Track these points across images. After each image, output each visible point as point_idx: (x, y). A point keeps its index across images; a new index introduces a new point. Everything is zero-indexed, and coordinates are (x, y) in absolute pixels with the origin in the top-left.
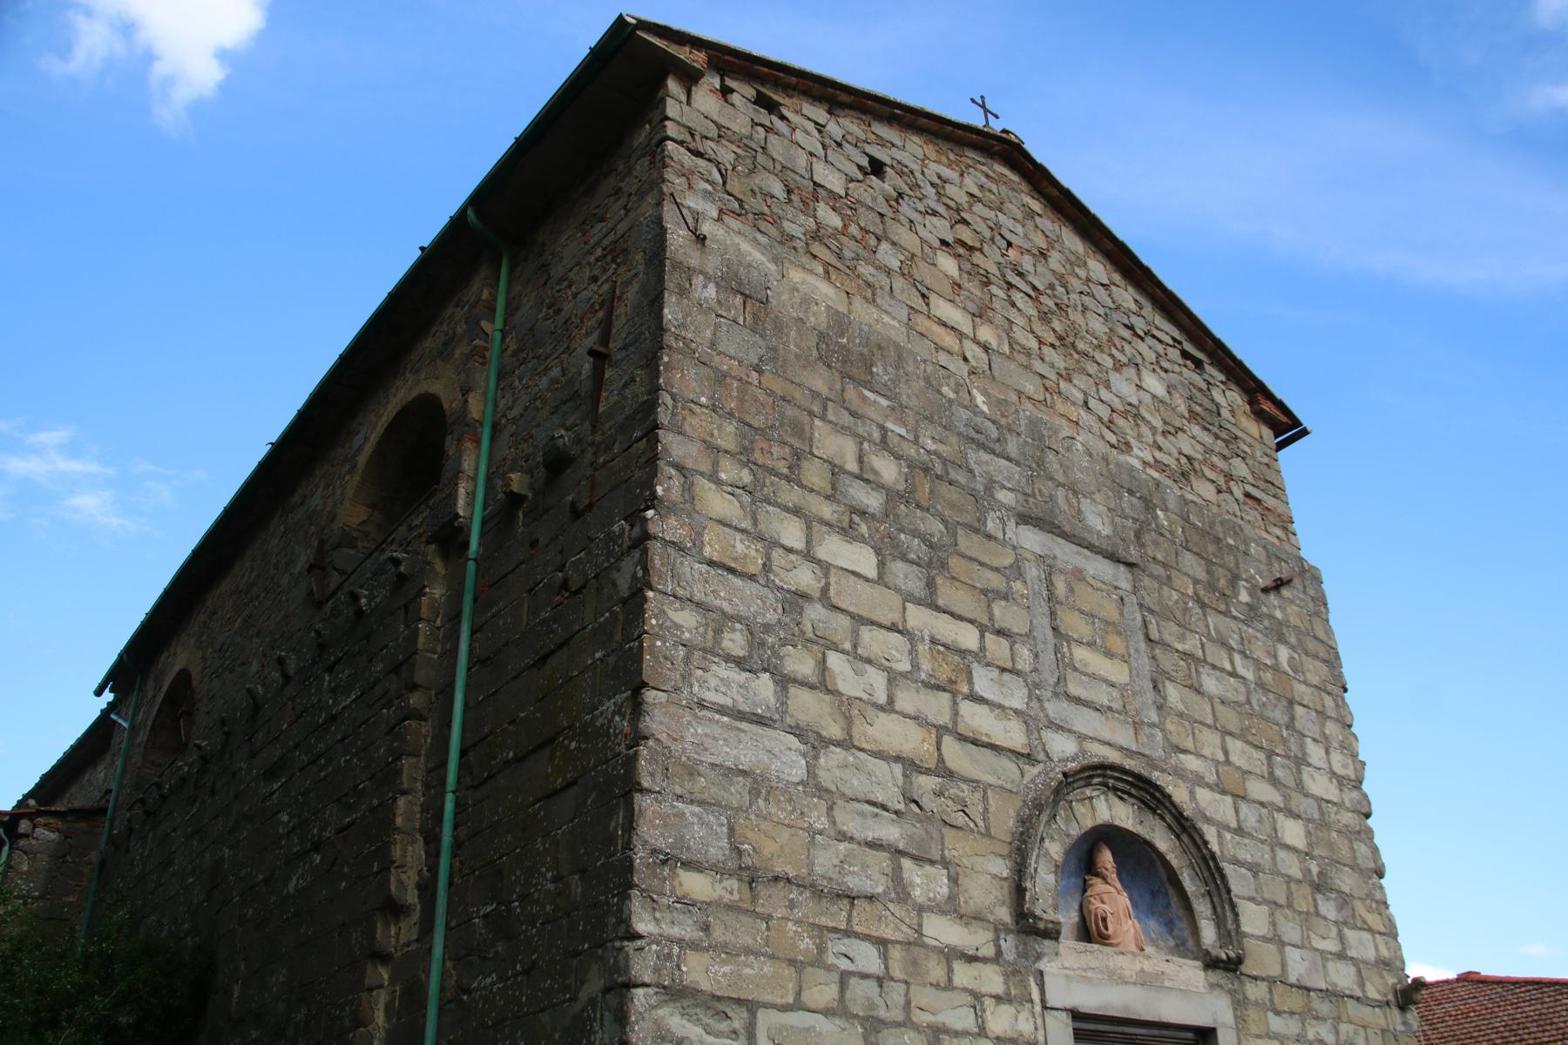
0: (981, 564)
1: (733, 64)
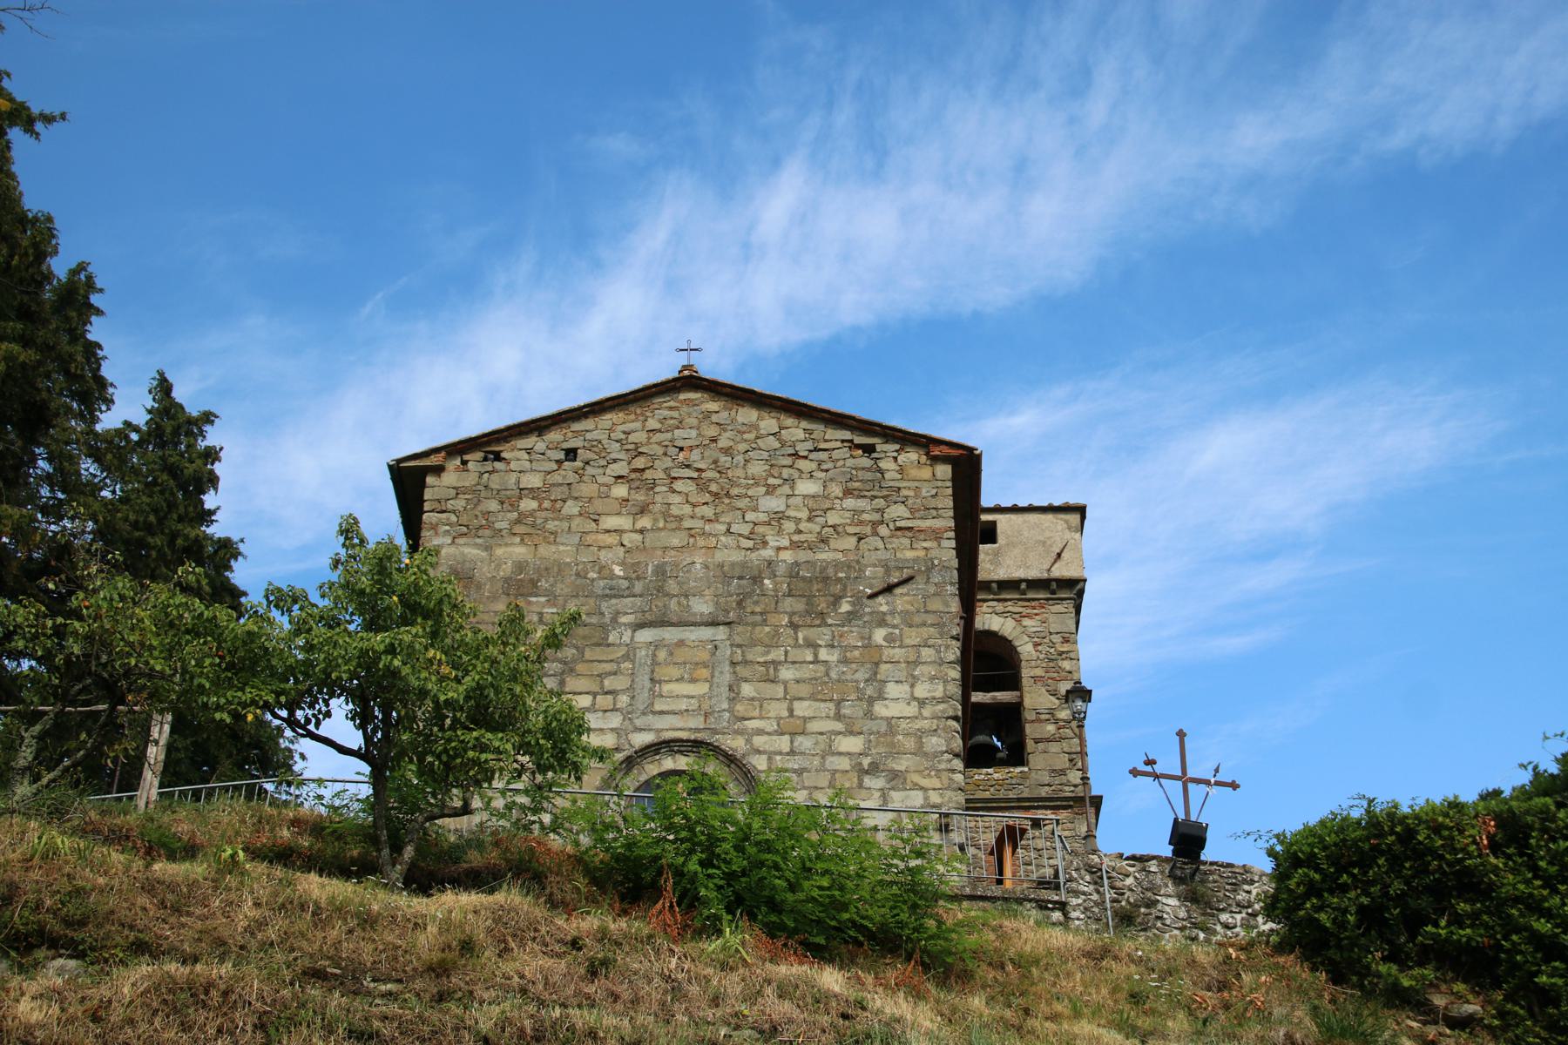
1: (459, 449)
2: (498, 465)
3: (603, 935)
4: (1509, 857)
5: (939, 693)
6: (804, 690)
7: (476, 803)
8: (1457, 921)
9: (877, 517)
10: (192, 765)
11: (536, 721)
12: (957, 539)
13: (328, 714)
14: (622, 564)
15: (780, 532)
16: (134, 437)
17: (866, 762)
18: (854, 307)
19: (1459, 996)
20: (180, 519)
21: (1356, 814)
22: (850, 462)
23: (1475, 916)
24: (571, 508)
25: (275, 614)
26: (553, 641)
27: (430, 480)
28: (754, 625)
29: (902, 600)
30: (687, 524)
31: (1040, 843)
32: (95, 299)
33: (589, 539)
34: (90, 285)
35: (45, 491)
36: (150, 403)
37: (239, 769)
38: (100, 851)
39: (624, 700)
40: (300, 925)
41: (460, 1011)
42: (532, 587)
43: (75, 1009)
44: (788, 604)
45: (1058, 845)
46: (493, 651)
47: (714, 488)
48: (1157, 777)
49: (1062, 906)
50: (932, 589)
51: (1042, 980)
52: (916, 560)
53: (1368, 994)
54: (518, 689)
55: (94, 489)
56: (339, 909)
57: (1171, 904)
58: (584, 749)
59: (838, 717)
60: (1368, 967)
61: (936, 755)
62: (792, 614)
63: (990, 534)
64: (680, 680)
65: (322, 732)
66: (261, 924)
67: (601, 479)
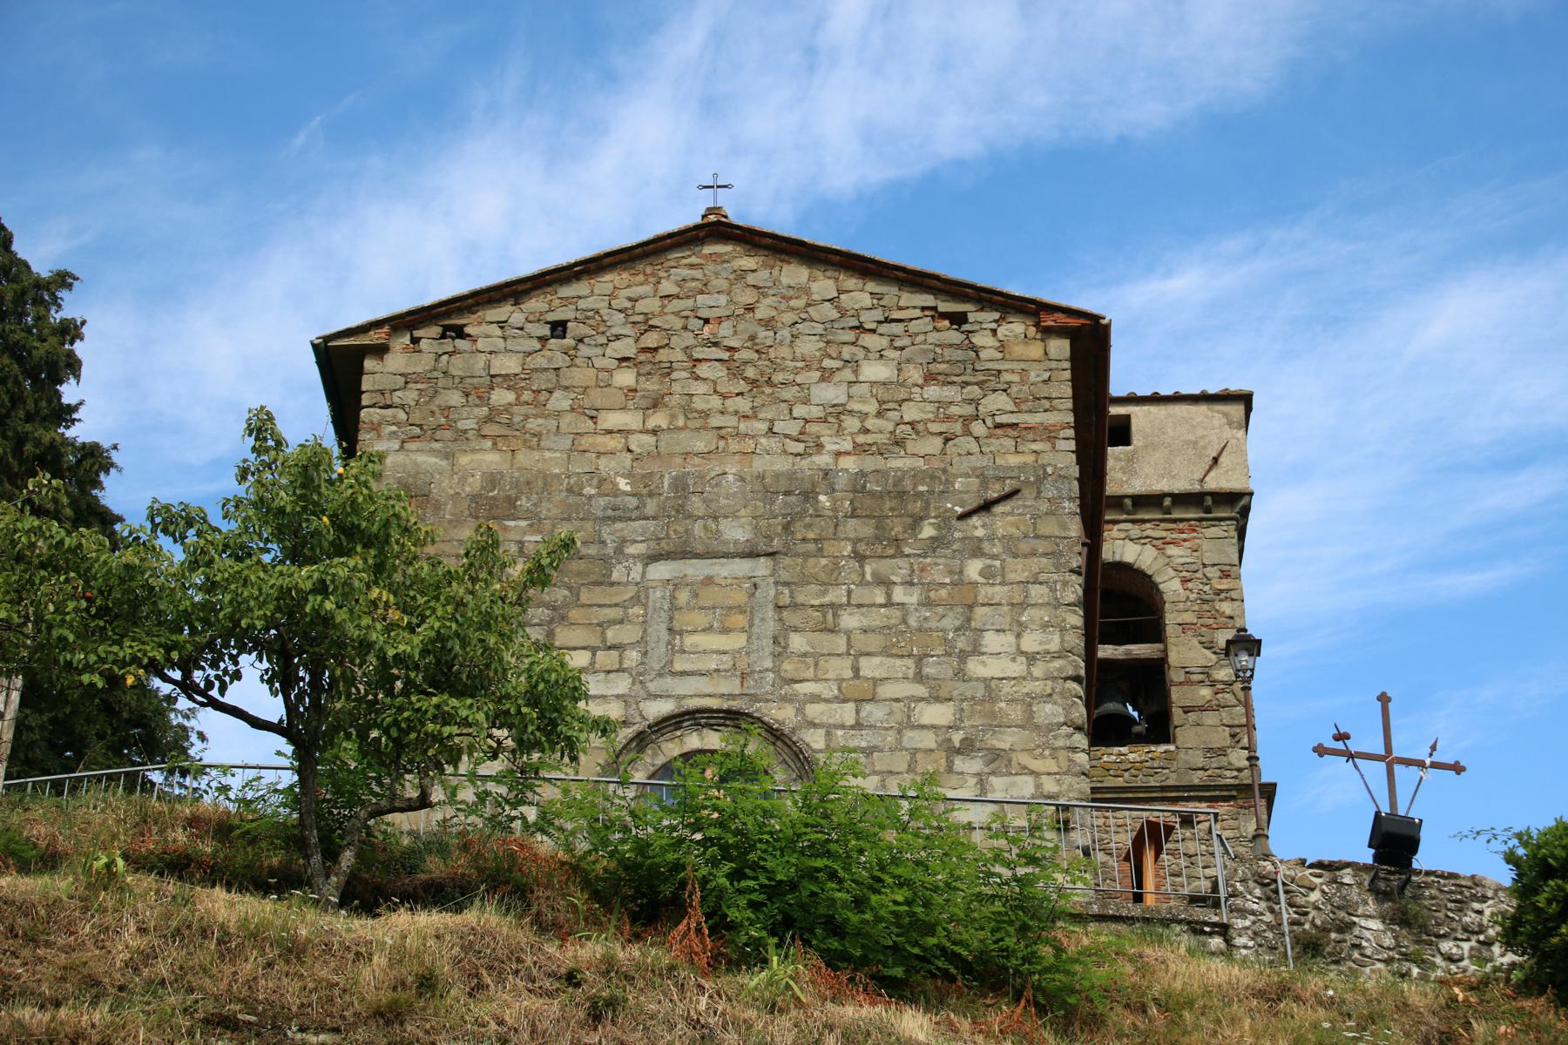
0: (600, 606)
1: (409, 322)
2: (461, 344)
3: (608, 967)
5: (1054, 646)
6: (874, 642)
7: (437, 794)
9: (969, 410)
12: (1078, 438)
13: (237, 676)
14: (629, 475)
17: (957, 738)
18: (955, 133)
20: (29, 418)
22: (933, 337)
24: (560, 401)
25: (164, 542)
26: (538, 576)
27: (369, 364)
28: (806, 556)
29: (1004, 520)
30: (715, 421)
31: (1192, 847)
33: (585, 442)
37: (116, 752)
39: (633, 656)
40: (201, 957)
42: (509, 507)
44: (852, 527)
45: (1218, 849)
46: (458, 590)
47: (750, 372)
49: (1223, 930)
51: (1197, 1027)
52: (1022, 467)
54: (492, 640)
57: (1372, 927)
58: (582, 720)
59: (919, 678)
61: (1052, 727)
62: (856, 541)
63: (1121, 433)
64: (708, 629)
65: (230, 698)
66: (148, 956)
67: (599, 362)
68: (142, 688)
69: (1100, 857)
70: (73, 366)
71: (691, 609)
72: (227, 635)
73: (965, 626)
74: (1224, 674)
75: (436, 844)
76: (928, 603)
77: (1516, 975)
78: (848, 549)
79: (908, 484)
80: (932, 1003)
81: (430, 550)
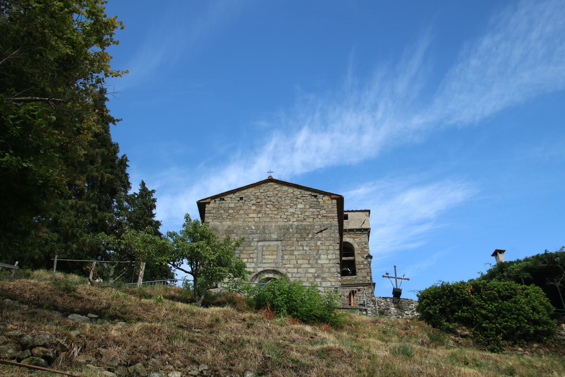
1: (214, 198)
2: (223, 202)
3: (251, 318)
4: (476, 295)
5: (334, 257)
6: (300, 257)
7: (219, 286)
8: (463, 311)
9: (318, 213)
10: (150, 276)
11: (233, 265)
12: (338, 219)
13: (183, 263)
14: (254, 226)
15: (294, 217)
16: (136, 196)
17: (316, 275)
18: (319, 163)
19: (464, 330)
20: (147, 216)
21: (438, 285)
22: (311, 200)
23: (467, 310)
24: (242, 212)
25: (169, 238)
26: (238, 245)
27: (207, 205)
28: (288, 241)
29: (324, 234)
30: (270, 215)
31: (360, 295)
32: (127, 163)
33: (246, 220)
34: (126, 160)
35: (116, 210)
36: (140, 188)
37: (161, 277)
38: (129, 296)
39: (255, 260)
40: (177, 315)
41: (216, 335)
42: (232, 232)
43: (124, 333)
44: (296, 235)
45: (365, 295)
46: (222, 247)
47: (277, 206)
48: (389, 277)
49: (366, 310)
50: (332, 231)
51: (361, 328)
52: (328, 224)
53: (442, 330)
54: (229, 256)
55: (126, 209)
56: (186, 311)
57: (393, 309)
58: (246, 272)
59: (309, 264)
60: (442, 323)
61: (334, 273)
62: (297, 238)
63: (346, 217)
64: (269, 255)
65: (181, 267)
66: (167, 314)
67: (249, 205)
68: (166, 265)
69: (343, 297)
70: (155, 207)
71: (266, 251)
72: (181, 255)
73: (317, 254)
74: (366, 262)
75: (219, 295)
76: (310, 250)
77: (419, 317)
78: (295, 240)
79: (306, 227)
80: (311, 324)
81: (217, 240)
